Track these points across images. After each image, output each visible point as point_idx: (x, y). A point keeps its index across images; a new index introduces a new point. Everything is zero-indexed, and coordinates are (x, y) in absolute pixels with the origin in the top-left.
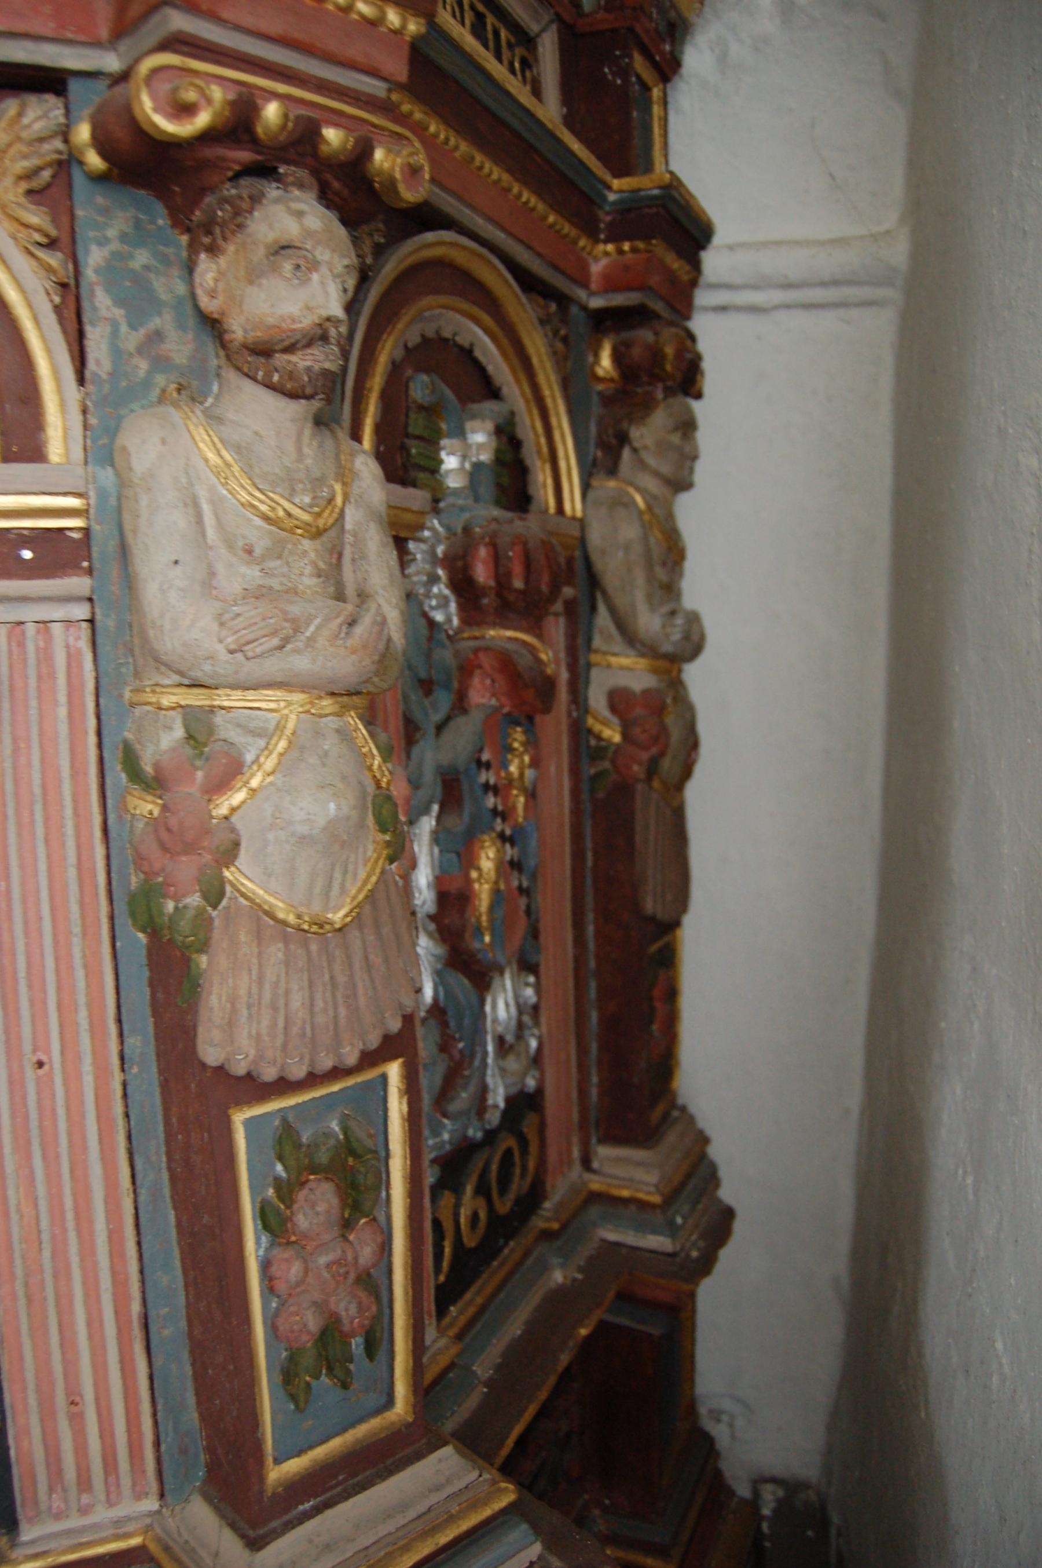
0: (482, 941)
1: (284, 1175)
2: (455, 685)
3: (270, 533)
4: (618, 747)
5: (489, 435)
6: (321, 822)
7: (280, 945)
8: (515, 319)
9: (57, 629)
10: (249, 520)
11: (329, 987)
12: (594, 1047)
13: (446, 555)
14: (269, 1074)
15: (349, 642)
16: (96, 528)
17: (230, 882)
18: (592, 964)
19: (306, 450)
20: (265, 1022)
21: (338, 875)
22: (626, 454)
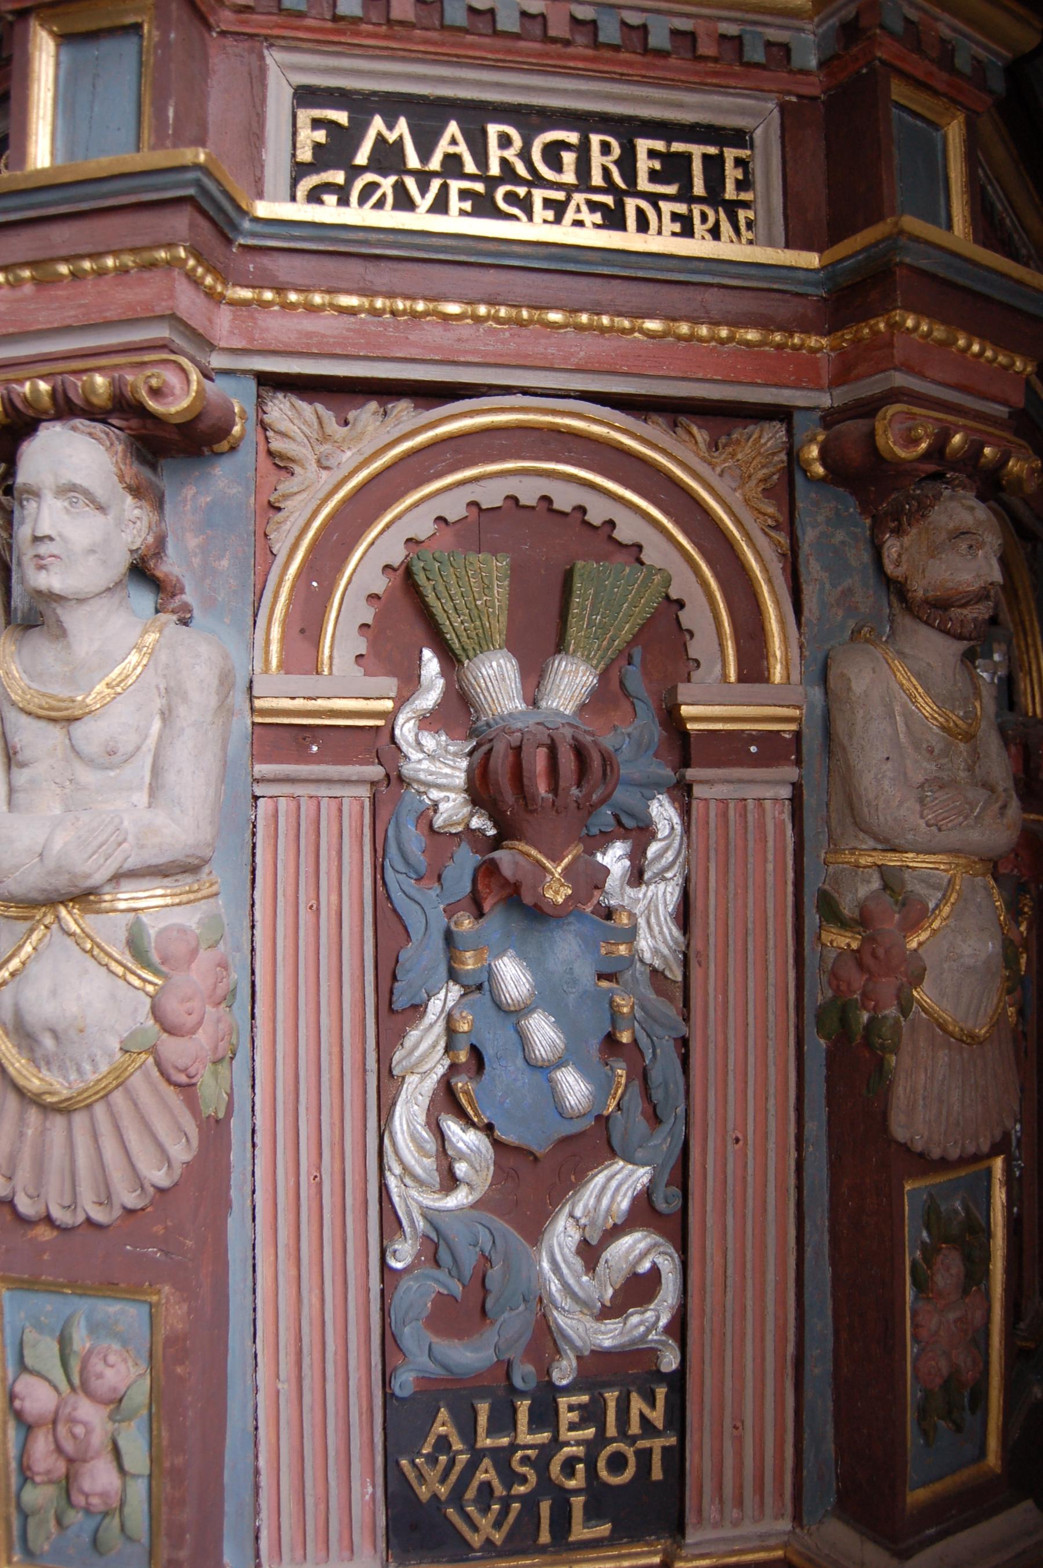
1: (928, 1240)
7: (946, 1051)
9: (768, 804)
14: (936, 1153)
15: (1005, 821)
16: (806, 731)
17: (918, 1002)
19: (958, 677)
21: (985, 1000)
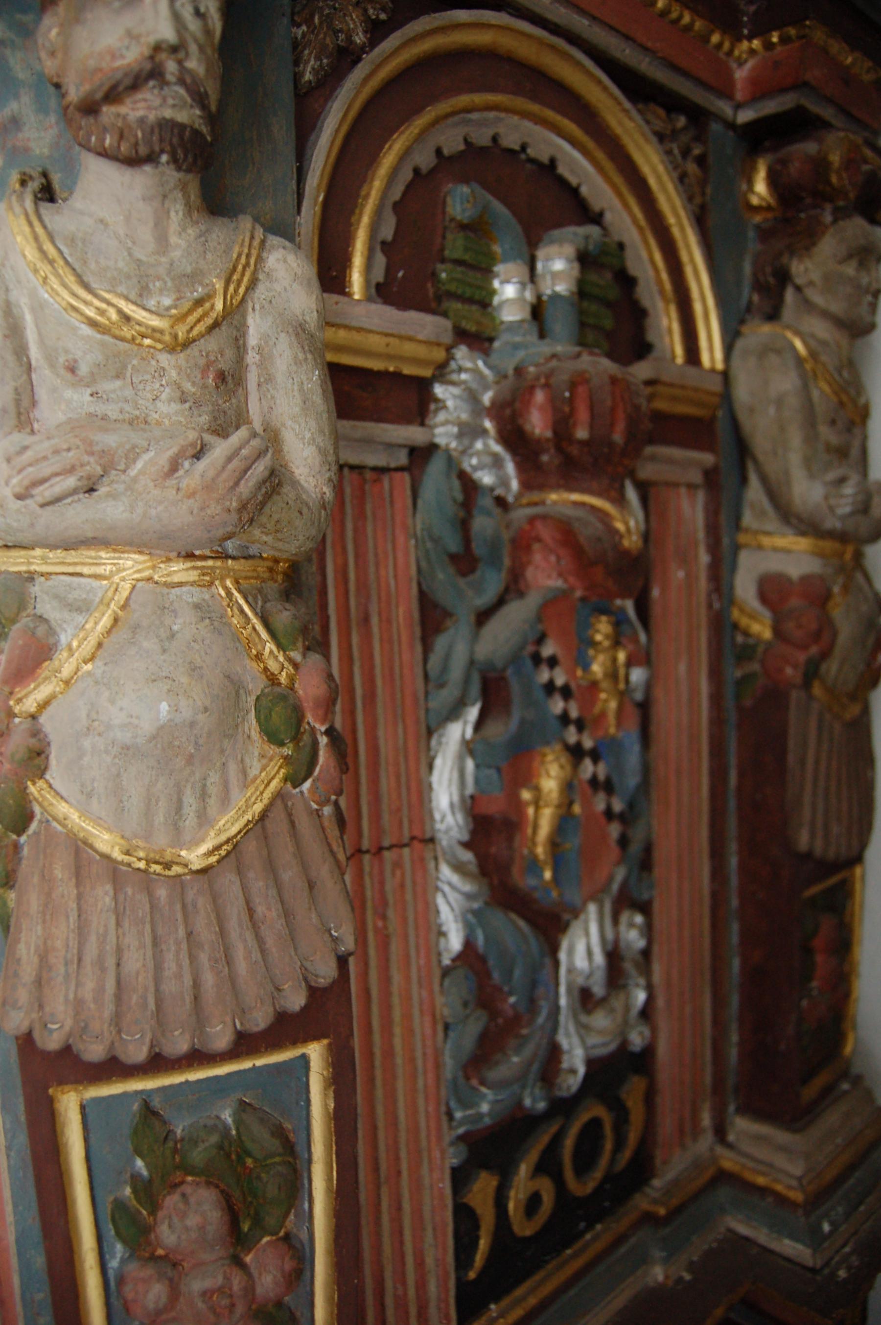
0: (540, 876)
1: (145, 1173)
2: (507, 562)
3: (103, 344)
4: (769, 644)
5: (569, 260)
6: (147, 727)
7: (109, 887)
8: (619, 131)
10: (75, 329)
11: (184, 946)
12: (735, 1000)
13: (493, 402)
14: (94, 1052)
18: (735, 902)
19: (174, 239)
20: (90, 985)
22: (789, 295)
